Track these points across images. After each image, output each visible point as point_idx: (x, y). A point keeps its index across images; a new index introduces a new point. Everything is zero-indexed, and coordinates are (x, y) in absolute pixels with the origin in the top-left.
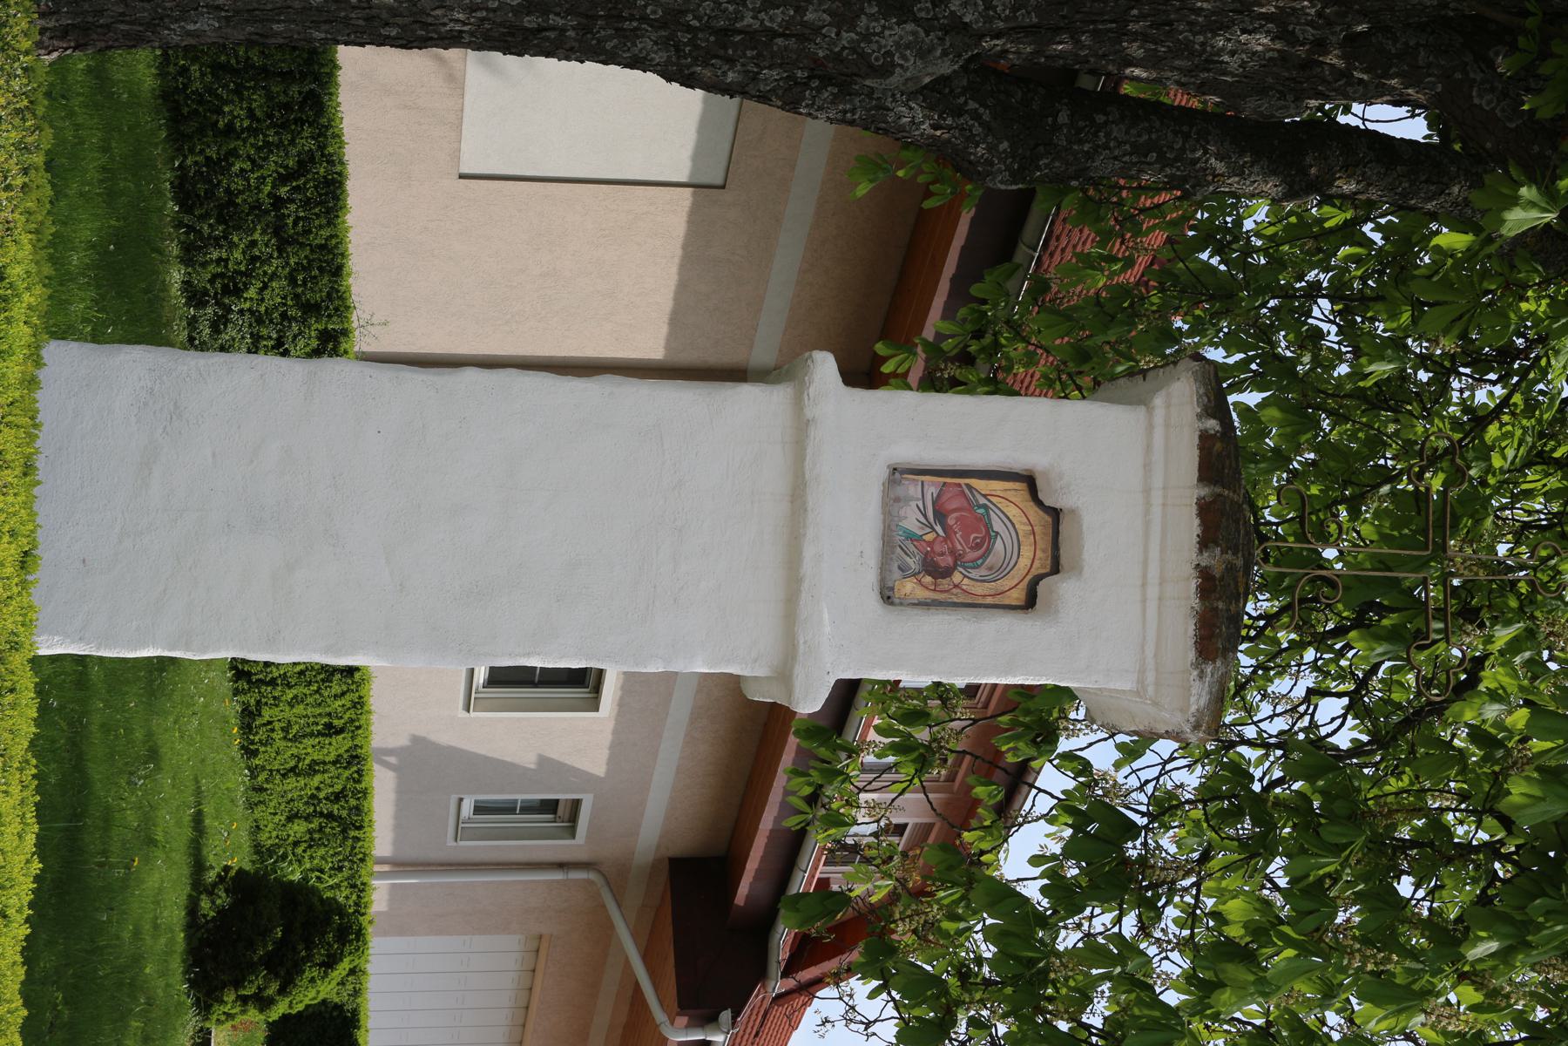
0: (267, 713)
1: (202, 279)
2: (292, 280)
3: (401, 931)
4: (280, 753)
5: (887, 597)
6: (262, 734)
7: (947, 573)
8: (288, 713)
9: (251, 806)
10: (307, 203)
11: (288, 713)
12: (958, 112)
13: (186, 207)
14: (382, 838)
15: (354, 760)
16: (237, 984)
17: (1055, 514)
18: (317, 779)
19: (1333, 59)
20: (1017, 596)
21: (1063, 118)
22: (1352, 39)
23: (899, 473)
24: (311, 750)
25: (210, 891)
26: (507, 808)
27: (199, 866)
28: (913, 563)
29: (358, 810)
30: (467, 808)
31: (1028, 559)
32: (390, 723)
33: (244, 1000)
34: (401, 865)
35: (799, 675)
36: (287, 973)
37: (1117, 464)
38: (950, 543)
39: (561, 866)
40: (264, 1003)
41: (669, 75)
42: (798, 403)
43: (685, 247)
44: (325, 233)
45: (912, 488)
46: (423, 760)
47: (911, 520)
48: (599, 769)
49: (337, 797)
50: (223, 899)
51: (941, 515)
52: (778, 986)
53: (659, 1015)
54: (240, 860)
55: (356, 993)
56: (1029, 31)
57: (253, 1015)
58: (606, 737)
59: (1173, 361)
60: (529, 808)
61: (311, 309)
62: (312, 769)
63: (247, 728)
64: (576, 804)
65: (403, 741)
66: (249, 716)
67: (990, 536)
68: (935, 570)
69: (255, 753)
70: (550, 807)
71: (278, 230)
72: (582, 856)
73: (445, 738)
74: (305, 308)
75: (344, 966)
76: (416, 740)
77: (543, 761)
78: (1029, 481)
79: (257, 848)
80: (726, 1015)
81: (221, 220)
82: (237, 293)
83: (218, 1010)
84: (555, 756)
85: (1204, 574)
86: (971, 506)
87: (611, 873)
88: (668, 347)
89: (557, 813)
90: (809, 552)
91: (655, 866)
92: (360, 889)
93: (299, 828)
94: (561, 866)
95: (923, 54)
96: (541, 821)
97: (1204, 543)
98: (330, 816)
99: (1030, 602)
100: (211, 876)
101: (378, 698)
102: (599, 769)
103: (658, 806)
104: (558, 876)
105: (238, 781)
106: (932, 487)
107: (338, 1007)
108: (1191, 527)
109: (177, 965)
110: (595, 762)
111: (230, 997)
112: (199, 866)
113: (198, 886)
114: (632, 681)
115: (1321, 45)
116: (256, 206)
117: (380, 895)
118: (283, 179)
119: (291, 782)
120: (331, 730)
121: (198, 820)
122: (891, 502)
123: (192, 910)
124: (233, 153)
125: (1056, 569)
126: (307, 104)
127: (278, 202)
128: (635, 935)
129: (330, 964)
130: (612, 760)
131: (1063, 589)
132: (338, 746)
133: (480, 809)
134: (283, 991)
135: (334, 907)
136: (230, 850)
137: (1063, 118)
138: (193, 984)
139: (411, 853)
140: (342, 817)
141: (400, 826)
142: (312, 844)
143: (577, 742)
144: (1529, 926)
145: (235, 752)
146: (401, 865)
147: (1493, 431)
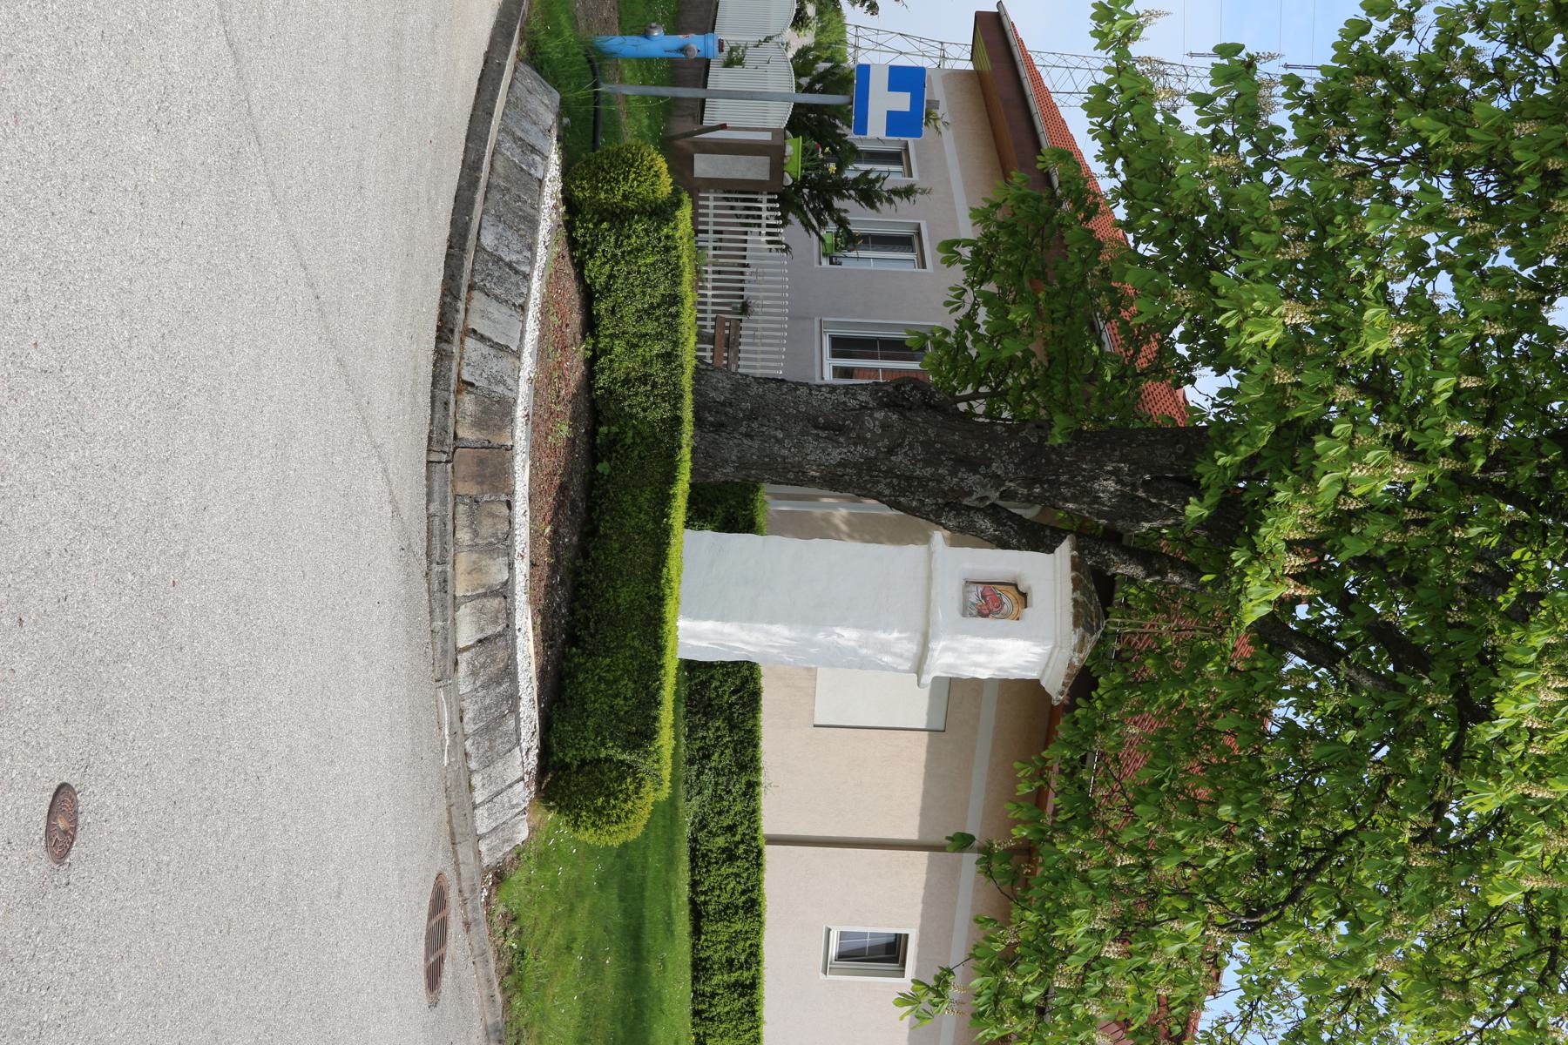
10: (744, 705)
22: (1145, 483)
23: (969, 583)
43: (926, 767)
44: (751, 722)
45: (973, 588)
47: (973, 598)
51: (984, 597)
61: (743, 767)
67: (1002, 604)
71: (729, 720)
81: (705, 714)
88: (920, 831)
90: (933, 592)
106: (980, 588)
108: (1070, 586)
118: (734, 693)
122: (966, 593)
124: (712, 677)
125: (1016, 586)
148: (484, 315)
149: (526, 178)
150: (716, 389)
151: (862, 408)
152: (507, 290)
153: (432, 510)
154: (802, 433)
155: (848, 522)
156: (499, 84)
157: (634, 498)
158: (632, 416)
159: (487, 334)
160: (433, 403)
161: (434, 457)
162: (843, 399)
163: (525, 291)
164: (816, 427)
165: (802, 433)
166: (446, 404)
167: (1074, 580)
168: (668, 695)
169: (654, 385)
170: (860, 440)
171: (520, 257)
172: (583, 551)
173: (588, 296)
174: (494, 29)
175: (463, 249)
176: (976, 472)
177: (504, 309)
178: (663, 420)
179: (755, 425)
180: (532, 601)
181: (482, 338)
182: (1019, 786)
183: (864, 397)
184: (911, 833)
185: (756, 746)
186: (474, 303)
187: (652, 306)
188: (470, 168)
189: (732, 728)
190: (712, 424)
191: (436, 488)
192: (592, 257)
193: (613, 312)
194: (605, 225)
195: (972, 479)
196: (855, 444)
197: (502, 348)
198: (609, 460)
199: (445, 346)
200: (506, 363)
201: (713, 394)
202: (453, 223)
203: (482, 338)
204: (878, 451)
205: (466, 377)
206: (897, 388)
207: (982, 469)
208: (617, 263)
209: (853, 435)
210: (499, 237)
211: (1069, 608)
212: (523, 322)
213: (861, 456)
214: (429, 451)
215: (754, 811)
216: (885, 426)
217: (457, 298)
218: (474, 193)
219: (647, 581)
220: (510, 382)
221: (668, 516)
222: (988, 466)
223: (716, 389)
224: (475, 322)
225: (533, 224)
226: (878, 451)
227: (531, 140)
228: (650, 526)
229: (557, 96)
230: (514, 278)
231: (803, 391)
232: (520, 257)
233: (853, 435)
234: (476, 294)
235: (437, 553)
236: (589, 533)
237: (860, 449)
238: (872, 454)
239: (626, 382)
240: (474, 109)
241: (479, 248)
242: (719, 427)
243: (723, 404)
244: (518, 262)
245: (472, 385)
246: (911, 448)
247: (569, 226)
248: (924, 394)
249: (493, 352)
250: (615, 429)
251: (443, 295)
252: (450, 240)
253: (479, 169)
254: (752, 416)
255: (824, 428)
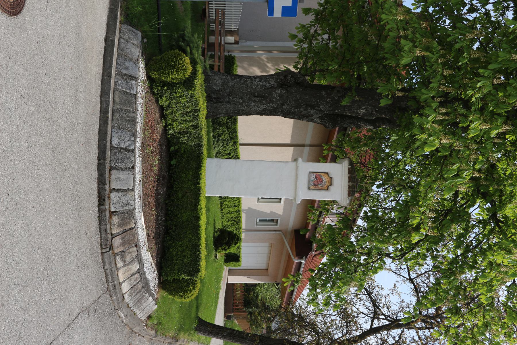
0: (224, 203)
1: (215, 134)
2: (229, 134)
3: (247, 242)
4: (226, 210)
5: (309, 189)
6: (224, 207)
7: (317, 185)
8: (228, 203)
9: (222, 219)
10: (232, 123)
11: (228, 203)
12: (324, 120)
13: (213, 124)
14: (243, 225)
15: (239, 211)
16: (221, 247)
17: (331, 178)
18: (232, 215)
19: (374, 113)
20: (326, 188)
21: (339, 119)
22: (376, 111)
23: (310, 172)
24: (231, 209)
25: (216, 232)
26: (265, 220)
27: (215, 228)
28: (312, 184)
29: (239, 220)
30: (258, 220)
31: (328, 183)
32: (244, 206)
33: (222, 249)
34: (247, 230)
35: (297, 199)
36: (229, 245)
37: (339, 171)
38: (318, 181)
39: (275, 231)
40: (225, 250)
41: (283, 117)
42: (297, 164)
43: (293, 125)
45: (312, 174)
46: (250, 211)
47: (312, 179)
48: (281, 213)
49: (236, 218)
50: (218, 233)
51: (316, 178)
52: (314, 253)
53: (293, 257)
54: (220, 227)
55: (239, 252)
56: (331, 110)
57: (224, 252)
58: (282, 208)
59: (345, 158)
60: (269, 220)
61: (232, 138)
62: (232, 213)
63: (221, 206)
64: (278, 220)
65: (247, 208)
66: (221, 204)
67: (322, 181)
68: (315, 185)
69: (222, 210)
70: (273, 220)
71: (227, 127)
72: (279, 229)
73: (254, 208)
74: (237, 157)
75: (238, 245)
76: (249, 208)
77: (271, 212)
78: (327, 173)
79: (223, 226)
80: (304, 257)
82: (221, 136)
83: (218, 251)
84: (273, 211)
85: (349, 186)
86: (320, 177)
87: (284, 232)
89: (275, 221)
90: (298, 183)
91: (292, 231)
92: (240, 234)
93: (230, 223)
94: (275, 231)
95: (317, 114)
96: (271, 223)
97: (349, 182)
98: (235, 221)
99: (328, 189)
100: (216, 230)
101: (242, 201)
102: (281, 213)
103: (292, 221)
104: (274, 233)
105: (220, 214)
107: (236, 254)
108: (347, 180)
109: (212, 243)
110: (281, 213)
111: (220, 249)
112: (215, 228)
113: (215, 232)
114: (286, 200)
115: (372, 111)
116: (224, 123)
117: (243, 236)
118: (228, 119)
119: (228, 215)
120: (235, 206)
121: (214, 220)
123: (214, 235)
126: (235, 121)
127: (227, 123)
128: (289, 244)
129: (236, 244)
130: (283, 212)
131: (331, 188)
132: (236, 209)
133: (260, 220)
134: (228, 248)
135: (236, 235)
136: (219, 226)
137: (339, 119)
138: (214, 246)
139: (248, 228)
140: (237, 221)
141: (246, 226)
142: (232, 226)
143: (278, 209)
144: (400, 232)
145: (219, 210)
146: (247, 230)
147: (400, 163)
148: (117, 180)
149: (129, 97)
150: (216, 85)
151: (272, 87)
152: (126, 163)
153: (106, 267)
154: (250, 100)
155: (267, 58)
156: (113, 54)
157: (186, 175)
158: (183, 143)
159: (119, 188)
160: (100, 232)
161: (104, 251)
162: (264, 84)
163: (133, 159)
164: (255, 96)
165: (250, 100)
166: (106, 230)
167: (349, 178)
168: (203, 242)
169: (190, 134)
170: (271, 101)
171: (130, 142)
172: (168, 196)
173: (162, 109)
174: (108, 16)
175: (105, 159)
176: (314, 109)
177: (126, 172)
178: (195, 145)
179: (231, 98)
180: (150, 249)
181: (118, 190)
182: (324, 152)
183: (272, 82)
184: (288, 141)
185: (236, 133)
186: (113, 177)
187: (187, 112)
188: (104, 112)
189: (228, 129)
190: (215, 98)
191: (106, 260)
192: (161, 98)
193: (172, 113)
194: (165, 88)
195: (313, 112)
196: (269, 103)
197: (127, 190)
198: (175, 158)
199: (102, 207)
200: (130, 195)
201: (215, 87)
202: (99, 147)
203: (118, 190)
204: (278, 105)
205: (113, 210)
206: (285, 77)
207: (316, 108)
208: (172, 100)
209: (268, 100)
210: (120, 138)
211: (347, 188)
212: (134, 175)
213: (272, 107)
214: (102, 249)
215: (236, 149)
216: (280, 96)
217: (104, 184)
218: (107, 127)
219: (192, 210)
220: (131, 203)
221: (199, 183)
222: (319, 107)
223: (216, 85)
224: (115, 185)
225: (133, 121)
226: (278, 105)
227: (129, 72)
228: (193, 188)
229: (140, 34)
230: (128, 155)
231: (249, 81)
232: (130, 142)
233: (268, 100)
234: (113, 172)
235: (110, 280)
236: (170, 187)
237: (271, 104)
238: (276, 106)
239: (180, 133)
240: (103, 76)
241: (112, 147)
242: (218, 100)
243: (219, 91)
244: (129, 146)
245: (115, 212)
246: (290, 102)
247: (151, 88)
248: (295, 79)
249: (122, 194)
250: (177, 147)
251: (99, 185)
252: (98, 157)
253: (108, 112)
254: (230, 94)
255: (257, 97)
